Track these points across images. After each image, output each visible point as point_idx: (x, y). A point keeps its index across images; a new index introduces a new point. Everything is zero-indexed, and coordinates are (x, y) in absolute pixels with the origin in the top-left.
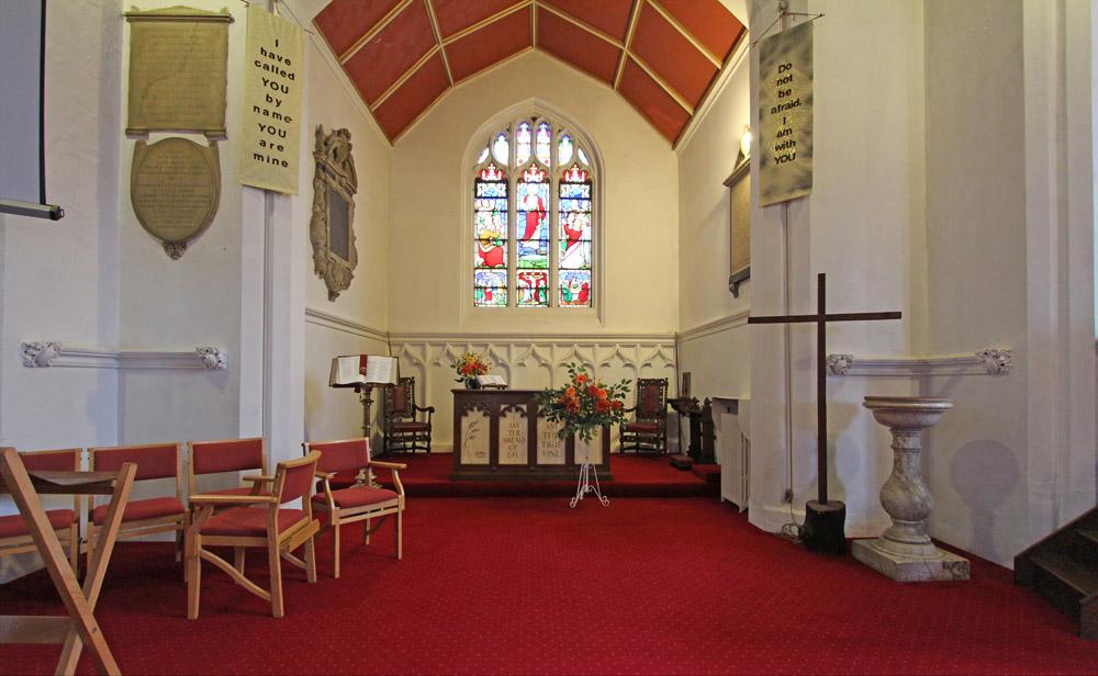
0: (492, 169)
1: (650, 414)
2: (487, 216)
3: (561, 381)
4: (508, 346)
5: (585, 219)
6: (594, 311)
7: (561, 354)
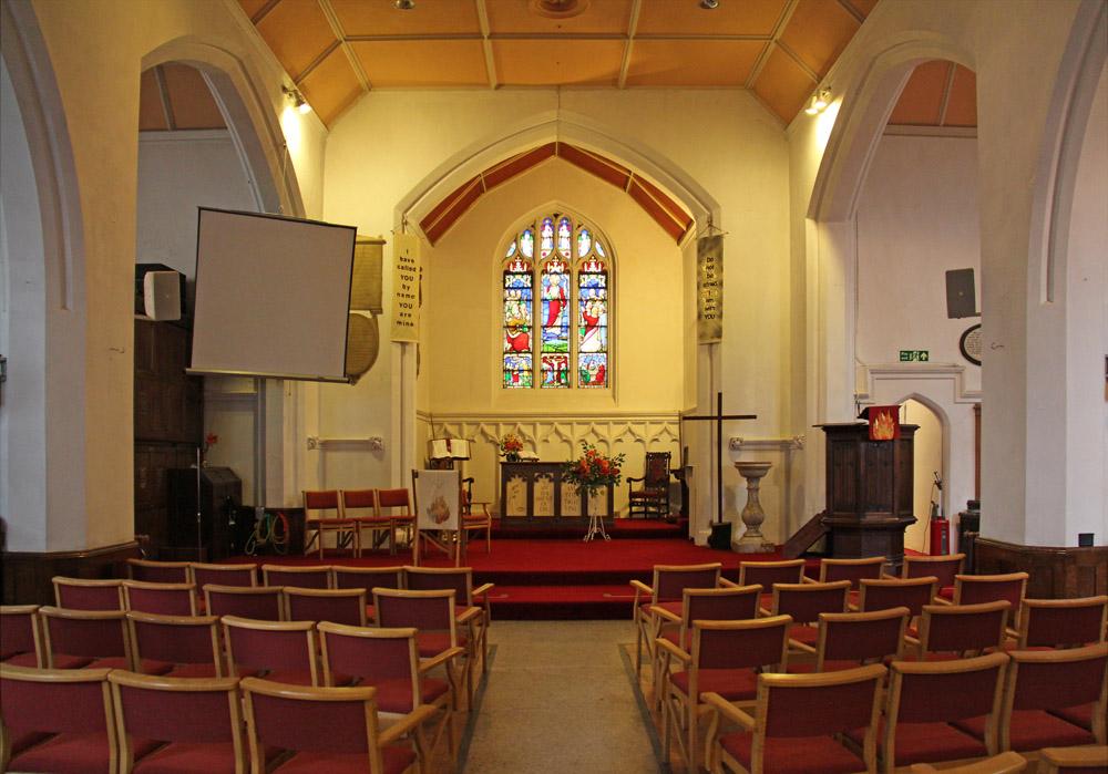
1: (658, 483)
3: (578, 454)
5: (600, 306)
6: (608, 391)
7: (580, 431)
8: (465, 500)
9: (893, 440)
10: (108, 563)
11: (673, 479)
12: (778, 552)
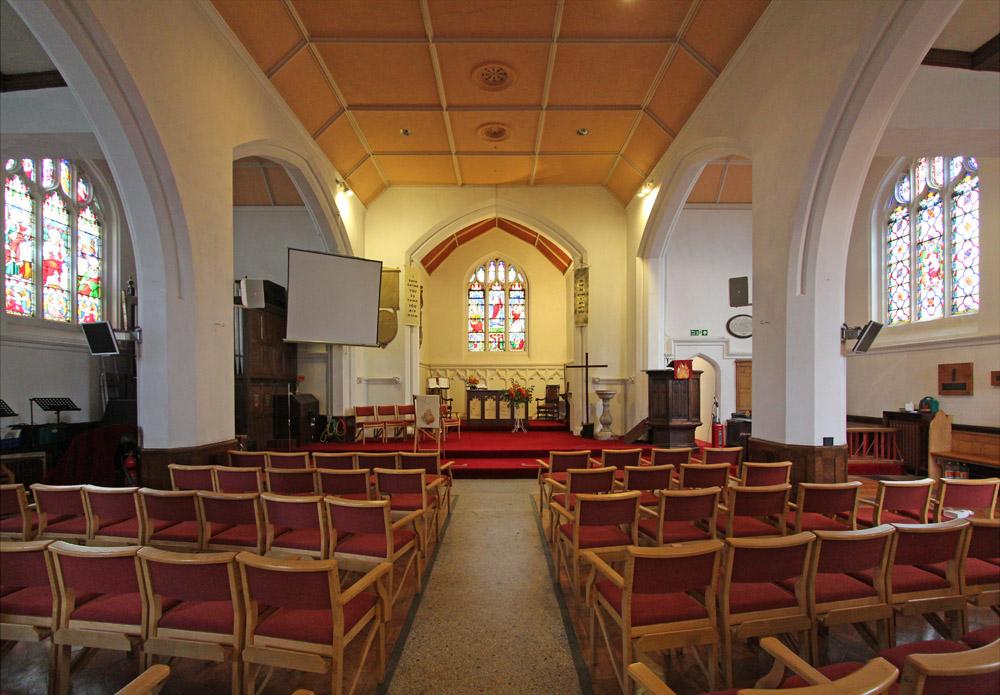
1: (552, 402)
2: (475, 307)
3: (509, 386)
4: (485, 370)
5: (523, 308)
6: (526, 353)
7: (510, 374)
8: (445, 411)
9: (688, 379)
10: (213, 454)
11: (561, 399)
12: (619, 441)
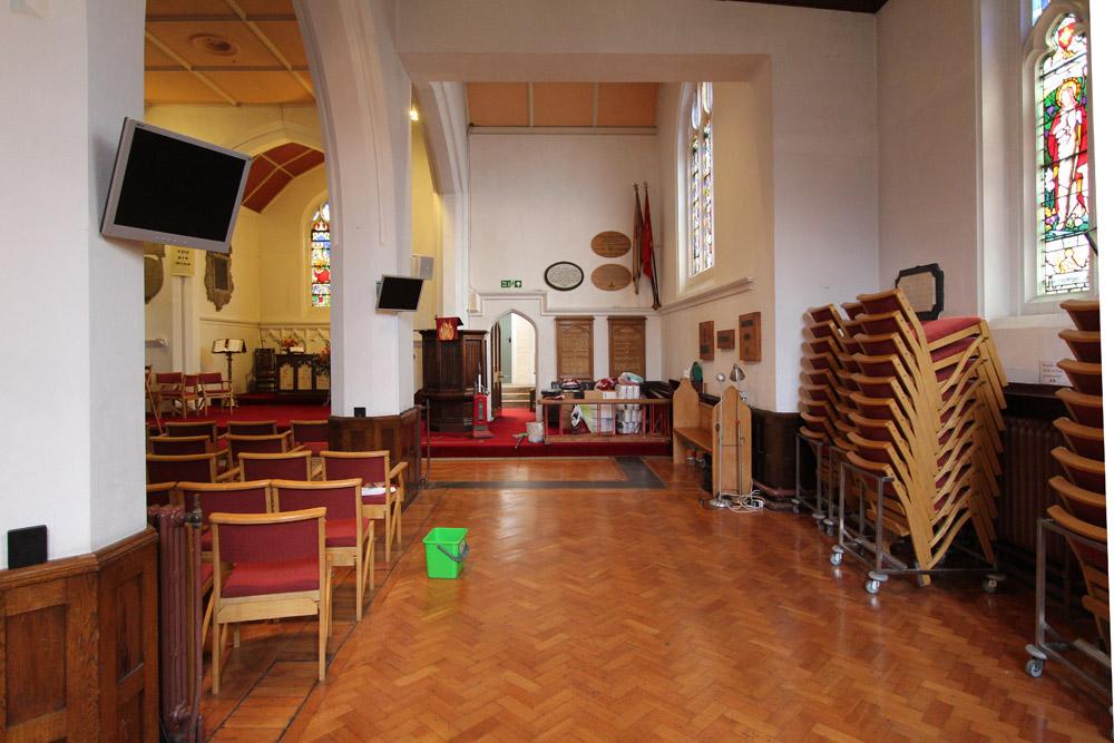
0: (321, 224)
2: (319, 252)
4: (304, 330)
